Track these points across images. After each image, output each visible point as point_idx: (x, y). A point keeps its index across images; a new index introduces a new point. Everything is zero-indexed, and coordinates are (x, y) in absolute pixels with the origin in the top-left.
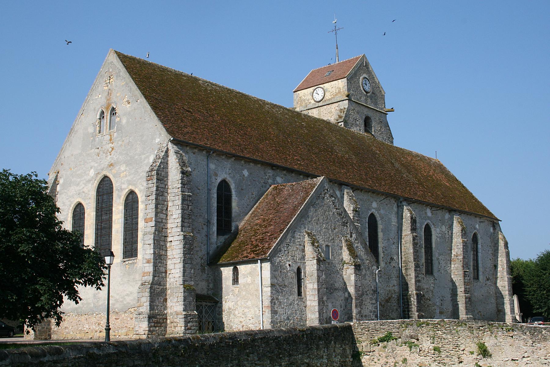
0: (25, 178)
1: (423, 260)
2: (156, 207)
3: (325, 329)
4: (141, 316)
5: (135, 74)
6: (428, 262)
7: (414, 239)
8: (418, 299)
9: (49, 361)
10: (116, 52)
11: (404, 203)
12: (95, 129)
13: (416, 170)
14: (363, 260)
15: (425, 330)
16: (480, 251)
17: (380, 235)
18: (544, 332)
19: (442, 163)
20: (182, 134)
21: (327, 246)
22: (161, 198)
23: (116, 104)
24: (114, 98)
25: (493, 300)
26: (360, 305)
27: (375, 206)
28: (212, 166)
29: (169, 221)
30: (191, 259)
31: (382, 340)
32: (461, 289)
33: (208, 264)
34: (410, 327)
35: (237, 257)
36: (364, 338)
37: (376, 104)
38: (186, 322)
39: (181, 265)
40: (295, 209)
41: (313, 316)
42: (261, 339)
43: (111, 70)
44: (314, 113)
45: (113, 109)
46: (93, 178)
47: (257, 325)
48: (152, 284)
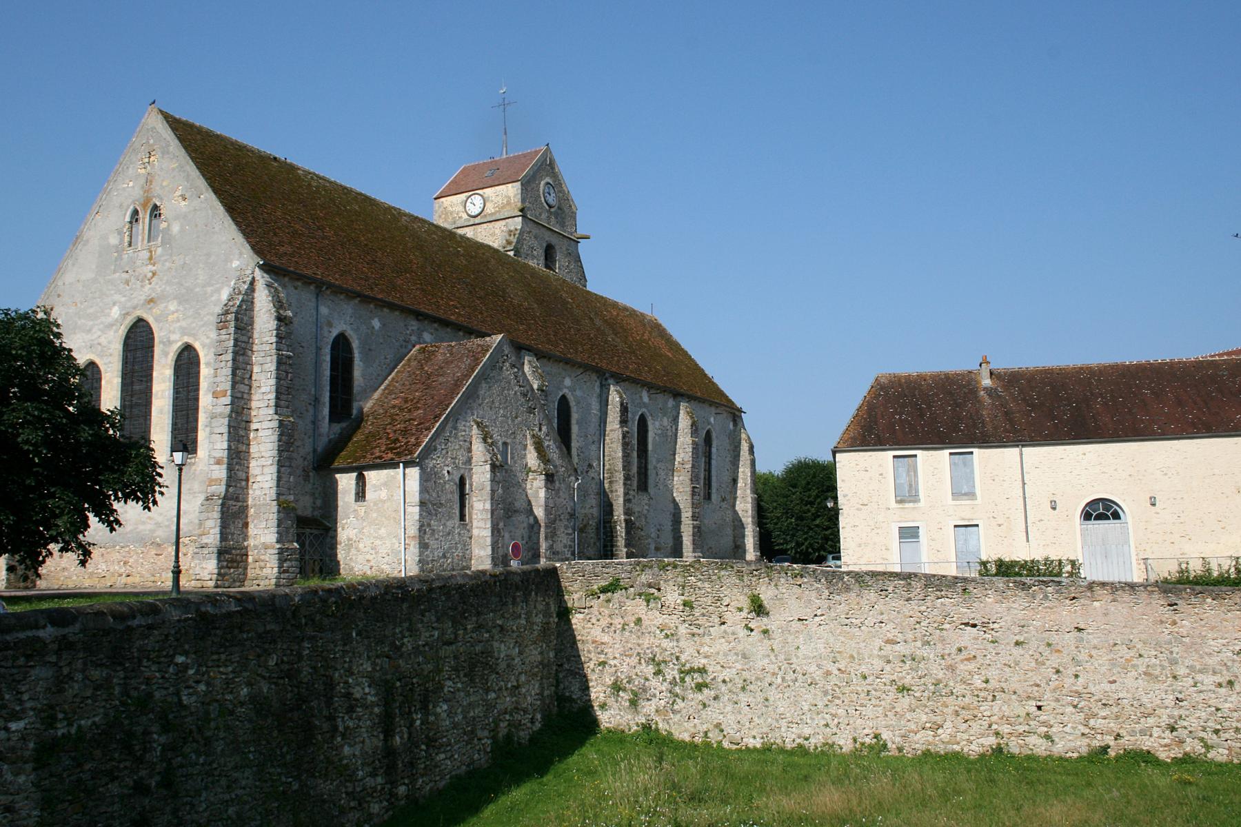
0: (25, 317)
1: (635, 469)
2: (234, 374)
3: (524, 573)
4: (206, 551)
5: (195, 151)
6: (641, 474)
7: (624, 437)
8: (626, 528)
9: (140, 626)
10: (161, 111)
11: (611, 381)
12: (122, 240)
13: (625, 330)
14: (555, 467)
15: (670, 574)
16: (714, 456)
17: (575, 429)
18: (846, 578)
19: (660, 321)
20: (276, 254)
21: (505, 444)
22: (241, 359)
23: (161, 199)
24: (156, 189)
25: (729, 531)
26: (551, 536)
27: (568, 384)
28: (324, 310)
29: (254, 397)
30: (290, 459)
31: (604, 590)
32: (686, 515)
33: (314, 469)
34: (648, 571)
35: (365, 457)
36: (576, 586)
37: (563, 225)
38: (281, 561)
39: (274, 469)
40: (457, 384)
41: (482, 553)
42: (440, 588)
43: (151, 142)
44: (469, 233)
45: (156, 207)
46: (116, 320)
47: (395, 565)
48: (224, 498)
